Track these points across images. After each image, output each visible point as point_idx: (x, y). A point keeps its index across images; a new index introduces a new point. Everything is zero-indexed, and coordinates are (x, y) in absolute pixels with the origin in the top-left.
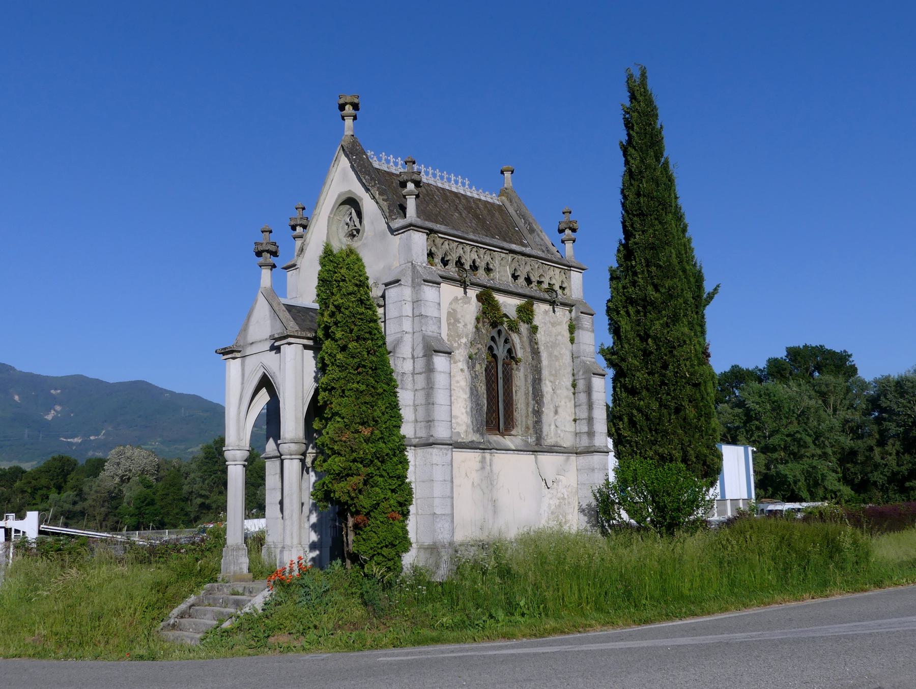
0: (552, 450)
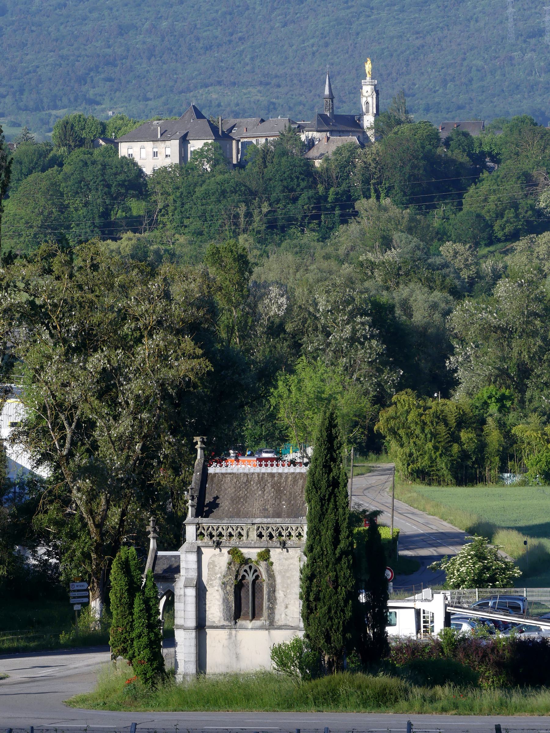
0: (280, 628)
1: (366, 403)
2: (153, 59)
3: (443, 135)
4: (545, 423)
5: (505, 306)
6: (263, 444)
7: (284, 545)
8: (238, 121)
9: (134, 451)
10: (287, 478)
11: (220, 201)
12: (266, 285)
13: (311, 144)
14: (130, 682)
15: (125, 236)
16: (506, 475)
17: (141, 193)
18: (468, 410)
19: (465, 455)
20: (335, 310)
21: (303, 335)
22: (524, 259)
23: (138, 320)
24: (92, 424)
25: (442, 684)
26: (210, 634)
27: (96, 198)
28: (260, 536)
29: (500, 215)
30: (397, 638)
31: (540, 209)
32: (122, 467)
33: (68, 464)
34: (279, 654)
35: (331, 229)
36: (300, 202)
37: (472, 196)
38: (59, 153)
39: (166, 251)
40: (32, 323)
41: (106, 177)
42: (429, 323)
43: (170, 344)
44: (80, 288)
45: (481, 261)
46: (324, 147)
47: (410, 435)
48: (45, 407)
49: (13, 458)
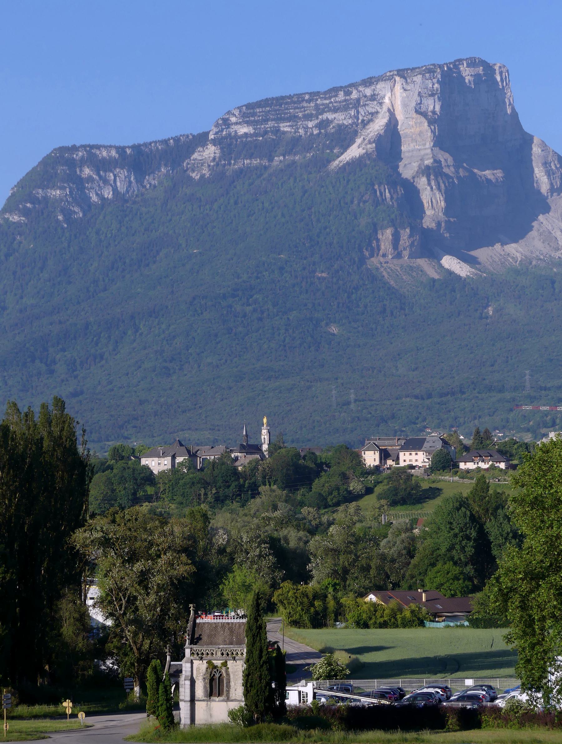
0: (232, 701)
1: (266, 588)
2: (156, 417)
3: (302, 454)
4: (356, 597)
5: (336, 538)
6: (215, 608)
7: (234, 659)
8: (199, 448)
9: (156, 612)
10: (236, 625)
11: (191, 487)
12: (217, 529)
13: (236, 459)
14: (157, 728)
15: (144, 504)
16: (338, 623)
17: (152, 483)
18: (318, 591)
19: (317, 613)
20: (251, 541)
21: (235, 554)
22: (343, 515)
23: (159, 546)
24: (135, 598)
25: (314, 728)
26: (197, 703)
27: (130, 485)
28: (222, 654)
29: (330, 493)
30: (290, 705)
31: (351, 490)
32: (151, 619)
33: (123, 618)
34: (232, 714)
35: (247, 501)
36: (231, 488)
37: (317, 484)
38: (111, 463)
39: (165, 512)
40: (105, 547)
41: (135, 475)
42: (297, 547)
43: (174, 558)
44: (130, 530)
45: (322, 516)
46: (243, 461)
47: (289, 603)
48: (112, 589)
49: (94, 617)
